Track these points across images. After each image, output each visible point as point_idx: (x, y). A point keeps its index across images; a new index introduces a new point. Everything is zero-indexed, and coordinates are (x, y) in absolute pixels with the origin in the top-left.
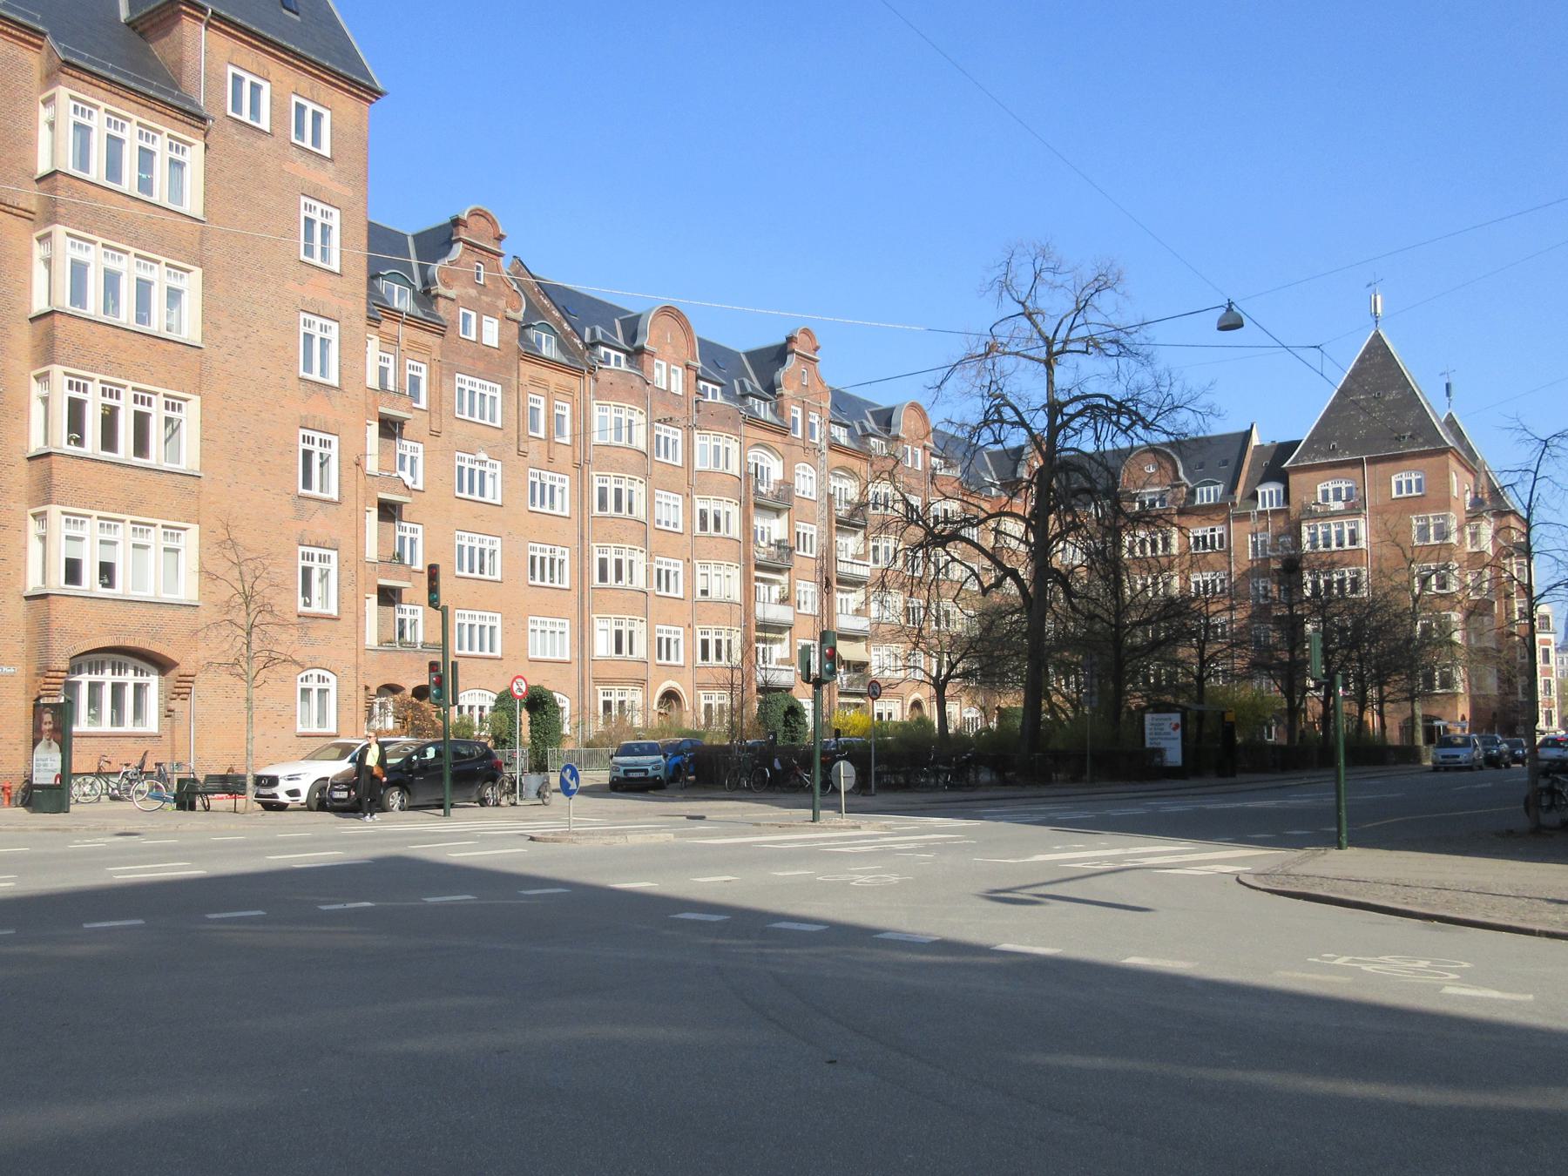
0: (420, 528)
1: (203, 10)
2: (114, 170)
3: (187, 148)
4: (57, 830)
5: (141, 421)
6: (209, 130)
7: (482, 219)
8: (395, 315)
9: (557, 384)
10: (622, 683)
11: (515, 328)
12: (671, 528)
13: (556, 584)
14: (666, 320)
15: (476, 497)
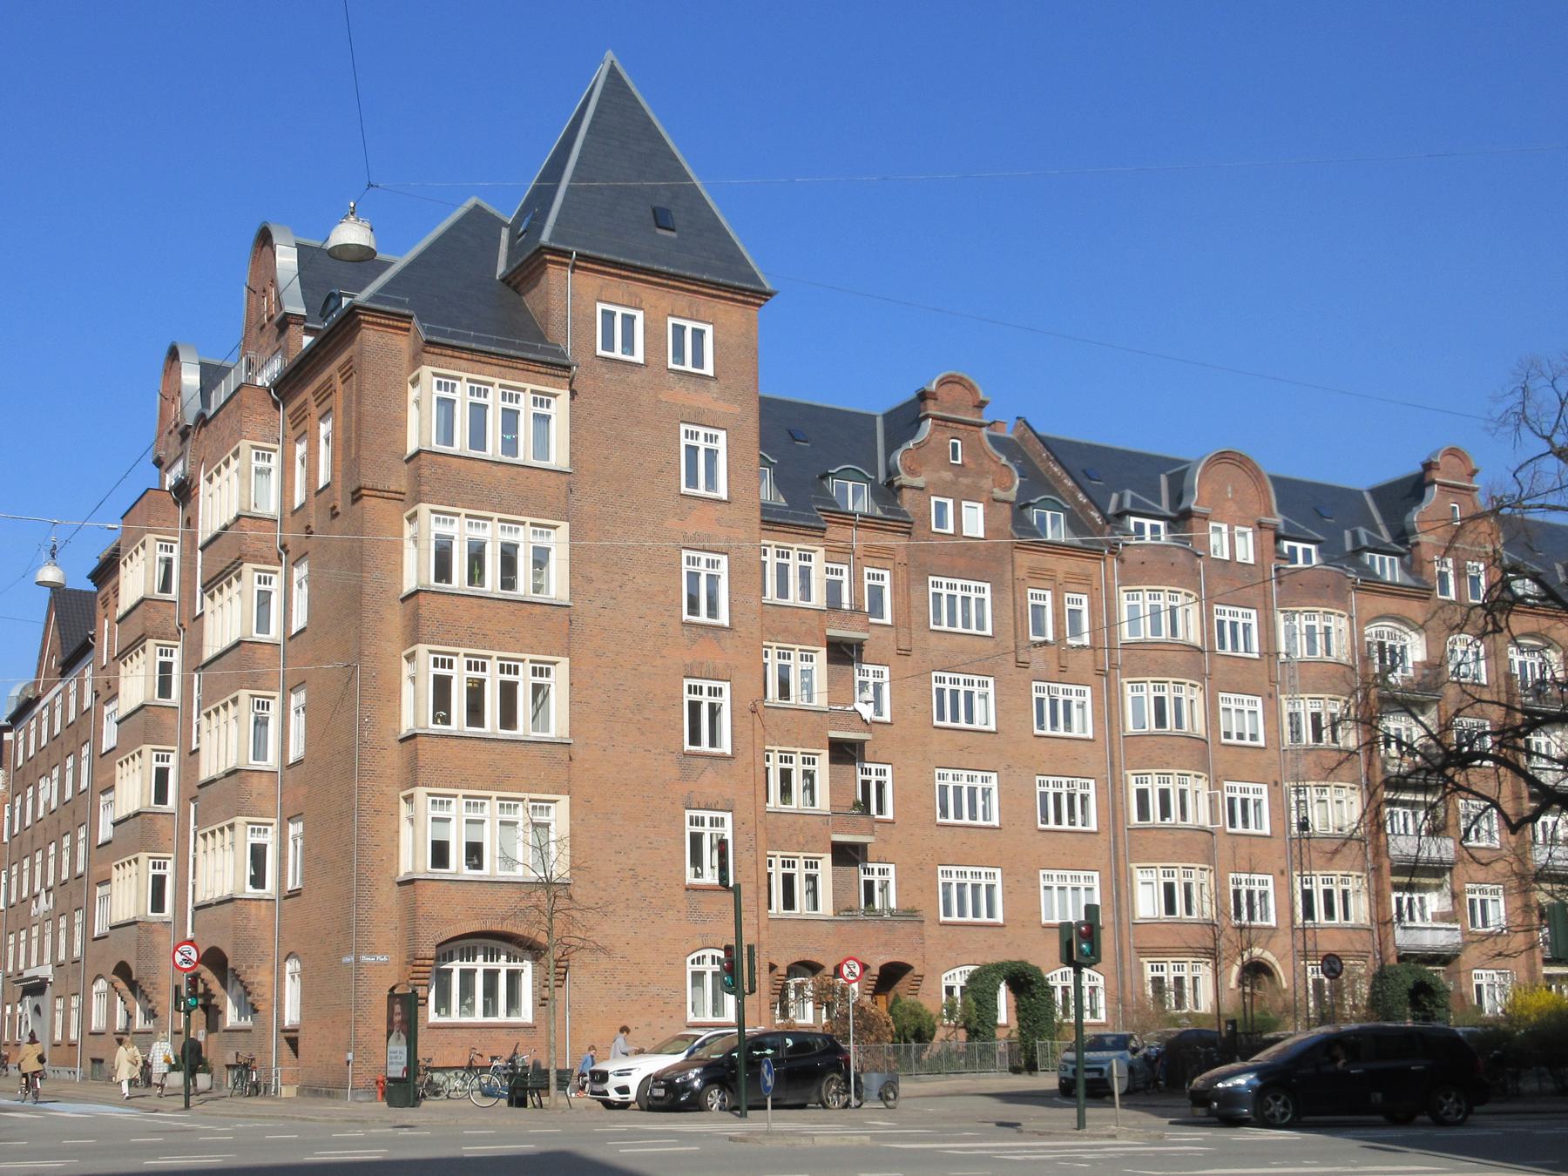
0: (889, 768)
1: (568, 254)
2: (478, 438)
3: (552, 399)
4: (356, 1121)
5: (508, 691)
6: (573, 377)
7: (957, 386)
8: (847, 519)
9: (1067, 573)
10: (1177, 954)
11: (1006, 511)
12: (1247, 742)
13: (1079, 827)
14: (1226, 469)
15: (962, 724)
